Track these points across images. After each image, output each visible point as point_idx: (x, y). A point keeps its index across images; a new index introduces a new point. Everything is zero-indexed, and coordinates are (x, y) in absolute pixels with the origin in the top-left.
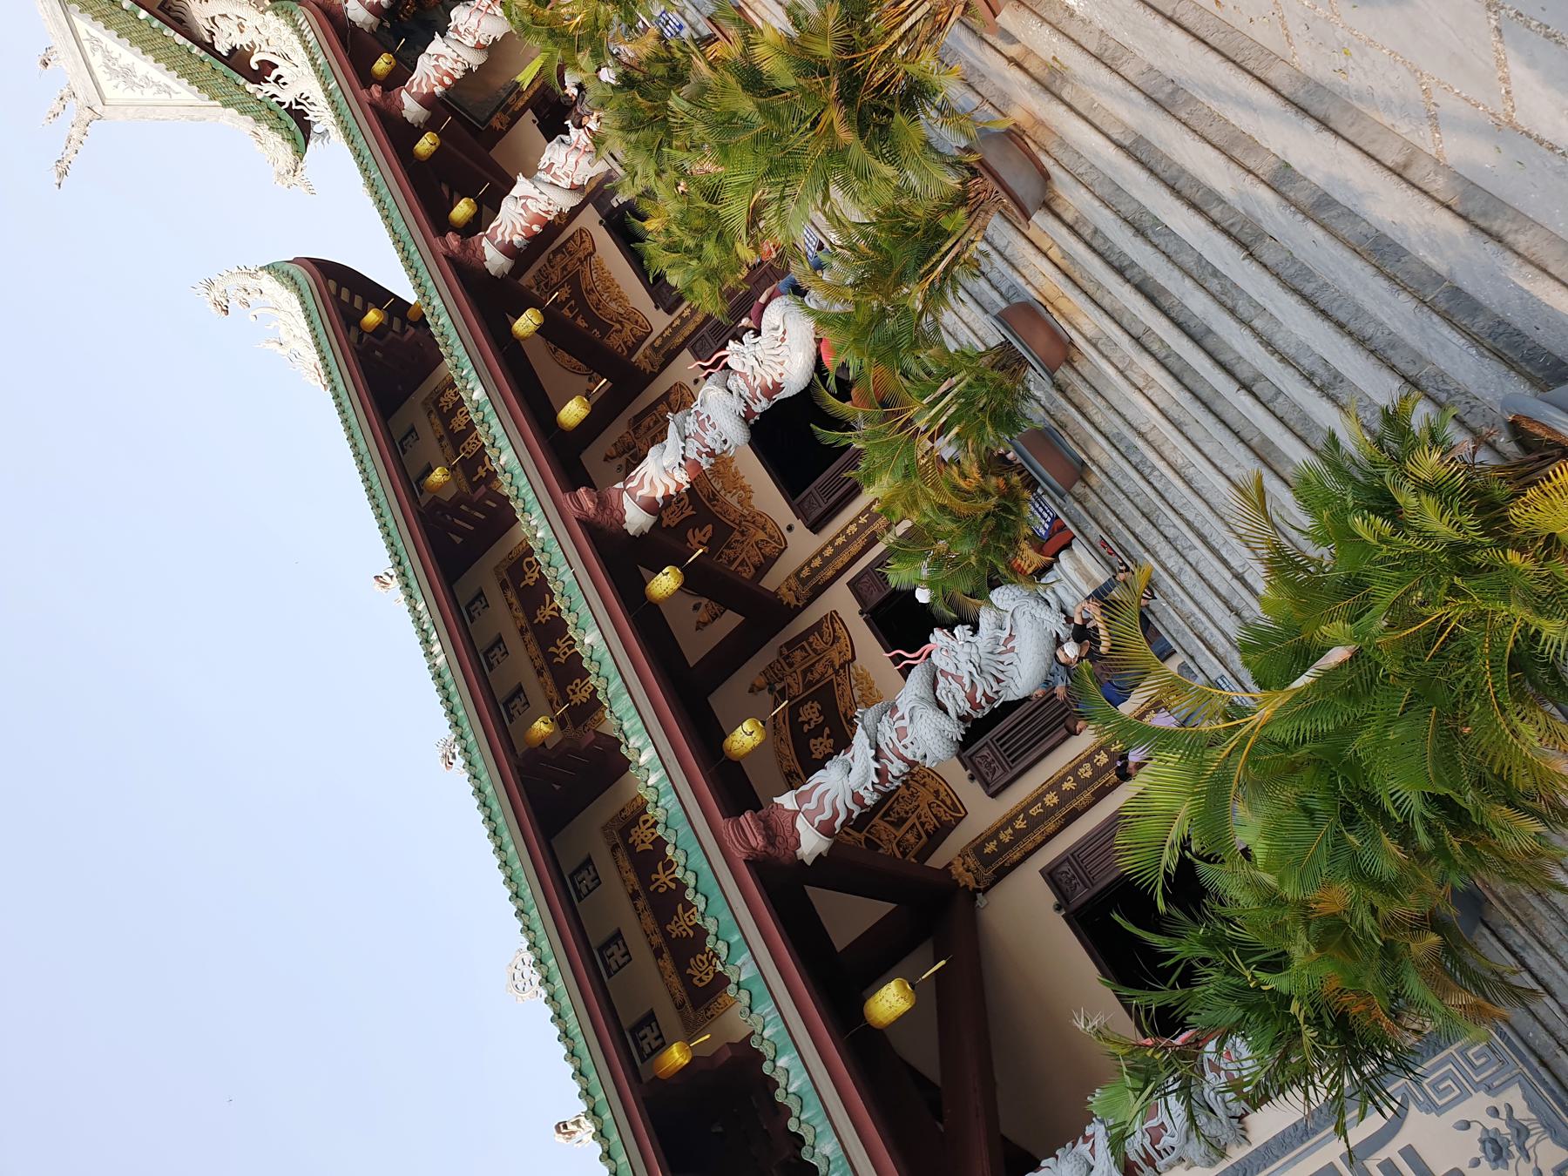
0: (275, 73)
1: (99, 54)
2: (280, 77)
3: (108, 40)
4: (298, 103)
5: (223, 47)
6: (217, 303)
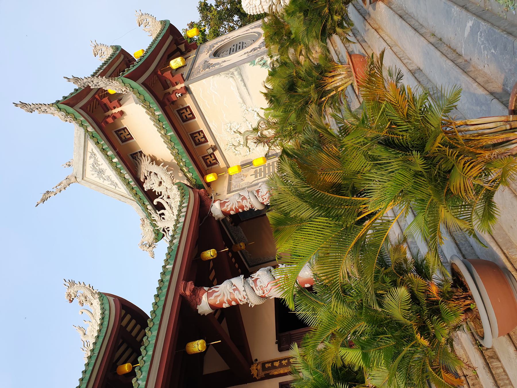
0: (162, 211)
1: (92, 160)
3: (100, 156)
4: (164, 230)
5: (147, 186)
6: (69, 295)
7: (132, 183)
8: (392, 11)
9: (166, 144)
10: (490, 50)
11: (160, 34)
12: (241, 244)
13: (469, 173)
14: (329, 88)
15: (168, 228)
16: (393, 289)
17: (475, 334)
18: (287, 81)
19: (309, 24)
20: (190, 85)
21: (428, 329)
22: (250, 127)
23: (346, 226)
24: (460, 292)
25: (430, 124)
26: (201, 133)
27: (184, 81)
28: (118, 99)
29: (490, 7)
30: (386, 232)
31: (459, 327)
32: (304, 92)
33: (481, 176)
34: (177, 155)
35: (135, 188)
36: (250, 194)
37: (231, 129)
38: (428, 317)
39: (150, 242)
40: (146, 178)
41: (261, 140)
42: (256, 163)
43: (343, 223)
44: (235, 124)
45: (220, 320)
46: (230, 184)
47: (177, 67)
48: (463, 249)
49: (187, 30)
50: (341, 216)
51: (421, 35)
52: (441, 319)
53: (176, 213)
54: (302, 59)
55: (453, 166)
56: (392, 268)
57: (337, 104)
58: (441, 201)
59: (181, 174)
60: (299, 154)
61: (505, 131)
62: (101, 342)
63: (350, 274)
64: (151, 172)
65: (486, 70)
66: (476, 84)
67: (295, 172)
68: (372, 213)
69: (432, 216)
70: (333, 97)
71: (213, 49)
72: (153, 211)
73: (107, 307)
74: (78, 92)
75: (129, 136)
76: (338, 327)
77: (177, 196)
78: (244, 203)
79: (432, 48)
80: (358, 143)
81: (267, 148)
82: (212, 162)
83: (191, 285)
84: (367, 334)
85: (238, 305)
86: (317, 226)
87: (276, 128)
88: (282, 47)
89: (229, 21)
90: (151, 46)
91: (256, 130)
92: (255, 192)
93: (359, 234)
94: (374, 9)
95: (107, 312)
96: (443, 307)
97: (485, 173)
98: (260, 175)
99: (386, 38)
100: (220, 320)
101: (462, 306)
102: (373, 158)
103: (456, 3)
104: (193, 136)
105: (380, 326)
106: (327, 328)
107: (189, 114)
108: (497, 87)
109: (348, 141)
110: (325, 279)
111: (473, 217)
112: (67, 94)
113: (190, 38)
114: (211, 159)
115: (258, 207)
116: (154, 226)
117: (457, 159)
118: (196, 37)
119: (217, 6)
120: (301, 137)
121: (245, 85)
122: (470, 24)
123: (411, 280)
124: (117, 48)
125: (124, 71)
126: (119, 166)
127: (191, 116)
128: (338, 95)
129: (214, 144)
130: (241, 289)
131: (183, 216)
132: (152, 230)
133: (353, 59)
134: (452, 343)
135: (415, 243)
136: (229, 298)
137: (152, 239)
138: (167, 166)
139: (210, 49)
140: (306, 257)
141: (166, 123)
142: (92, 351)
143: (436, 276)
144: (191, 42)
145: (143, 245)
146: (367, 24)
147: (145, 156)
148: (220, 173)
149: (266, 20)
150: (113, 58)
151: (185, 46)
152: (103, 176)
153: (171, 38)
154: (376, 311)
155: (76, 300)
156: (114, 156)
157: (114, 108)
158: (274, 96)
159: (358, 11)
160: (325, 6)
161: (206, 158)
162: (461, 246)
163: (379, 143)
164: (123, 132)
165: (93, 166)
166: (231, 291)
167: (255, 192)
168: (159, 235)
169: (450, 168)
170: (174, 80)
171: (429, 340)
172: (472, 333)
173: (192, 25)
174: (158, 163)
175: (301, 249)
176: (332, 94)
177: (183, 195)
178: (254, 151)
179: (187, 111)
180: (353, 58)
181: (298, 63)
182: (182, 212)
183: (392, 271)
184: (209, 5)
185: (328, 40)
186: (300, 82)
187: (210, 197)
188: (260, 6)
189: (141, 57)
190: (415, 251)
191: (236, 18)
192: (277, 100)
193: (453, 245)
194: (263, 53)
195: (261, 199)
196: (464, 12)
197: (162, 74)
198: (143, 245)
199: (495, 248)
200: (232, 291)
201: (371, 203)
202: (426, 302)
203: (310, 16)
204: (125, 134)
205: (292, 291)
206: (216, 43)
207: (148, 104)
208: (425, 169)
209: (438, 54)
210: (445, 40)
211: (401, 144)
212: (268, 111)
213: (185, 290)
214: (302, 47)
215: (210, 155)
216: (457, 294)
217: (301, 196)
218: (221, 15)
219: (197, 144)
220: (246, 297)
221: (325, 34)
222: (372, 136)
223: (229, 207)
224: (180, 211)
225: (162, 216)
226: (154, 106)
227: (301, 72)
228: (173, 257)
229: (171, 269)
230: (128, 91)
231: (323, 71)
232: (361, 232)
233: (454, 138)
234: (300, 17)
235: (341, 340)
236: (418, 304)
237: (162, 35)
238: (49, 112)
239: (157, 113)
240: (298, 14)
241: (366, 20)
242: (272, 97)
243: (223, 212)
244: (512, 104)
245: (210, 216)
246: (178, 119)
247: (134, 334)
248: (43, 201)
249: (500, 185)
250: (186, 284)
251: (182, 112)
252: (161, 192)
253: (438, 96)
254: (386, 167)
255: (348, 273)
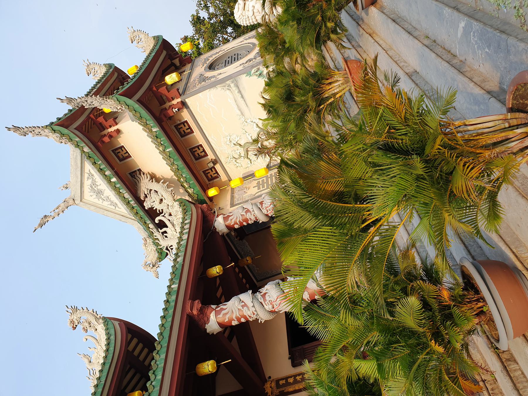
0: (164, 229)
1: (90, 181)
2: (165, 232)
4: (167, 249)
6: (72, 322)
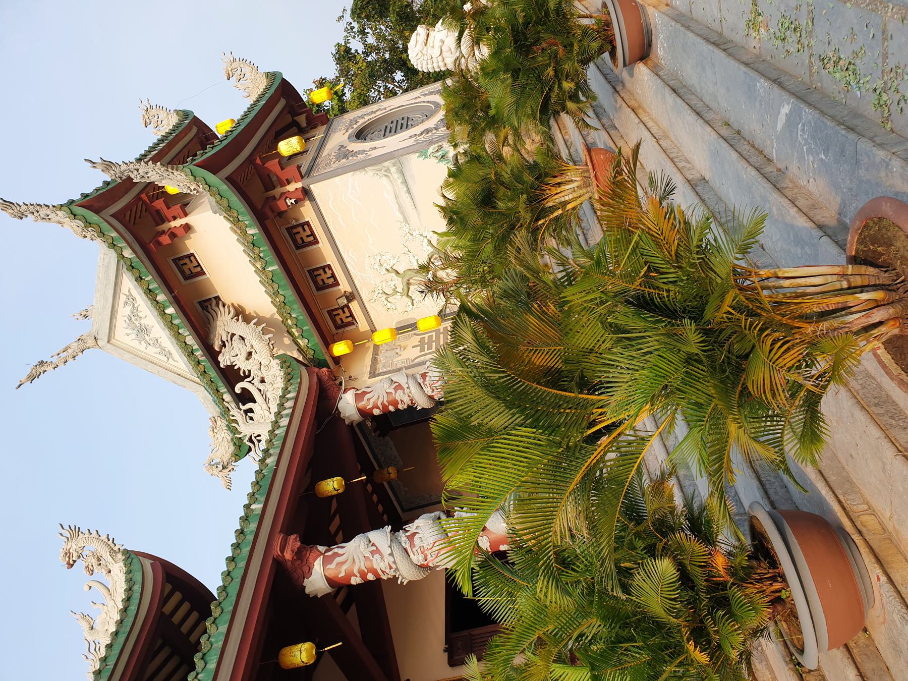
0: (249, 405)
3: (142, 302)
4: (251, 440)
5: (224, 360)
6: (68, 554)
7: (199, 353)
8: (659, 81)
9: (264, 285)
10: (818, 154)
11: (263, 94)
12: (390, 470)
13: (780, 360)
14: (551, 204)
15: (259, 436)
16: (649, 561)
17: (789, 643)
18: (480, 189)
19: (521, 93)
20: (312, 186)
21: (708, 634)
22: (415, 264)
23: (567, 446)
24: (763, 569)
25: (715, 273)
26: (327, 270)
27: (302, 177)
28: (183, 203)
29: (819, 84)
30: (637, 458)
31: (762, 630)
32: (508, 209)
33: (799, 367)
34: (282, 307)
35: (203, 361)
36: (410, 379)
37: (381, 265)
38: (708, 611)
39: (225, 460)
40: (224, 345)
41: (433, 286)
42: (422, 326)
43: (563, 439)
44: (389, 256)
45: (345, 607)
46: (375, 361)
47: (291, 153)
48: (771, 492)
49: (311, 90)
50: (558, 426)
51: (707, 122)
52: (731, 615)
53: (274, 409)
54: (506, 151)
55: (754, 346)
56: (648, 523)
57: (564, 232)
58: (730, 407)
59: (287, 341)
60: (491, 314)
61: (840, 292)
62: (122, 643)
63: (574, 532)
64: (233, 335)
65: (812, 187)
66: (795, 209)
67: (482, 345)
68: (614, 422)
69: (716, 434)
70: (557, 219)
71: (355, 126)
72: (233, 405)
73: (138, 577)
74: (110, 187)
75: (199, 269)
76: (551, 628)
77: (279, 379)
78: (399, 395)
79: (725, 145)
80: (591, 300)
81: (442, 300)
82: (345, 320)
83: (294, 542)
84: (601, 639)
85: (379, 580)
86: (517, 443)
87: (459, 267)
88: (473, 129)
89: (386, 80)
90: (245, 115)
91: (424, 268)
92: (418, 377)
93: (590, 460)
94: (632, 75)
95: (137, 588)
96: (736, 594)
97: (807, 362)
98: (430, 348)
99: (650, 124)
100: (345, 607)
101: (768, 592)
102: (618, 329)
103: (763, 75)
104: (313, 273)
105: (625, 626)
106: (530, 628)
107: (308, 236)
108: (828, 216)
109: (574, 296)
110: (530, 540)
111: (785, 438)
112: (88, 191)
113: (319, 105)
114: (343, 316)
115: (422, 403)
116: (234, 431)
117: (760, 335)
118: (326, 103)
119: (367, 54)
120: (498, 286)
121: (409, 191)
122: (785, 110)
123: (680, 548)
124: (186, 114)
125: (196, 155)
126: (176, 322)
127: (311, 238)
128: (567, 216)
129: (349, 290)
130: (386, 551)
131: (287, 415)
132: (229, 438)
133: (594, 157)
134: (749, 660)
135: (691, 477)
136: (363, 567)
137: (228, 456)
138: (264, 325)
139: (351, 126)
140: (496, 498)
141: (265, 249)
142: (104, 660)
143: (725, 537)
144: (318, 111)
145: (212, 465)
146: (619, 100)
147: (224, 306)
148: (358, 342)
149: (449, 82)
150: (177, 132)
151: (307, 118)
152: (147, 338)
153: (282, 103)
154: (616, 598)
155: (80, 564)
156: (168, 304)
157: (175, 218)
158: (456, 213)
159: (605, 76)
160: (549, 65)
161: (335, 313)
162: (768, 486)
163: (628, 302)
164: (187, 260)
165: (130, 319)
166: (368, 555)
167: (418, 377)
168: (241, 449)
169: (747, 351)
170: (283, 175)
171: (709, 654)
172: (785, 642)
173: (321, 83)
174: (247, 319)
175: (490, 482)
176: (555, 214)
177: (289, 377)
178: (420, 305)
179: (304, 230)
180: (593, 154)
181: (500, 158)
182: (285, 409)
183: (648, 529)
184: (353, 51)
185: (552, 122)
186: (502, 191)
187: (337, 382)
188: (440, 59)
189: (228, 132)
190: (689, 491)
191: (399, 76)
192: (462, 219)
193: (755, 483)
194: (441, 138)
195: (429, 389)
196: (776, 90)
197: (264, 164)
198: (212, 465)
199: (824, 492)
200: (368, 555)
201: (612, 405)
202: (705, 584)
203: (522, 80)
204: (191, 266)
205: (469, 563)
206: (362, 117)
207: (236, 215)
208: (705, 351)
209: (734, 155)
210: (745, 133)
211: (666, 305)
212: (445, 238)
213: (282, 550)
214: (507, 130)
215: (342, 308)
216: (759, 571)
217: (490, 387)
218: (373, 69)
219: (319, 289)
220: (394, 566)
221: (547, 112)
222: (618, 289)
223: (371, 402)
224: (281, 406)
225: (250, 414)
226: (245, 218)
227: (504, 173)
228: (265, 490)
229: (259, 512)
230: (201, 190)
231: (542, 174)
232: (593, 457)
233: (757, 299)
234: (505, 79)
235: (555, 651)
236: (692, 588)
237: (267, 96)
238: (53, 220)
239: (251, 231)
240: (502, 76)
241: (618, 92)
242: (452, 214)
243: (360, 410)
244: (852, 245)
245: (337, 417)
246: (287, 242)
247: (185, 629)
248: (31, 378)
249: (832, 383)
250: (286, 540)
251: (295, 231)
252: (249, 371)
253: (730, 225)
254: (639, 344)
255: (570, 530)
